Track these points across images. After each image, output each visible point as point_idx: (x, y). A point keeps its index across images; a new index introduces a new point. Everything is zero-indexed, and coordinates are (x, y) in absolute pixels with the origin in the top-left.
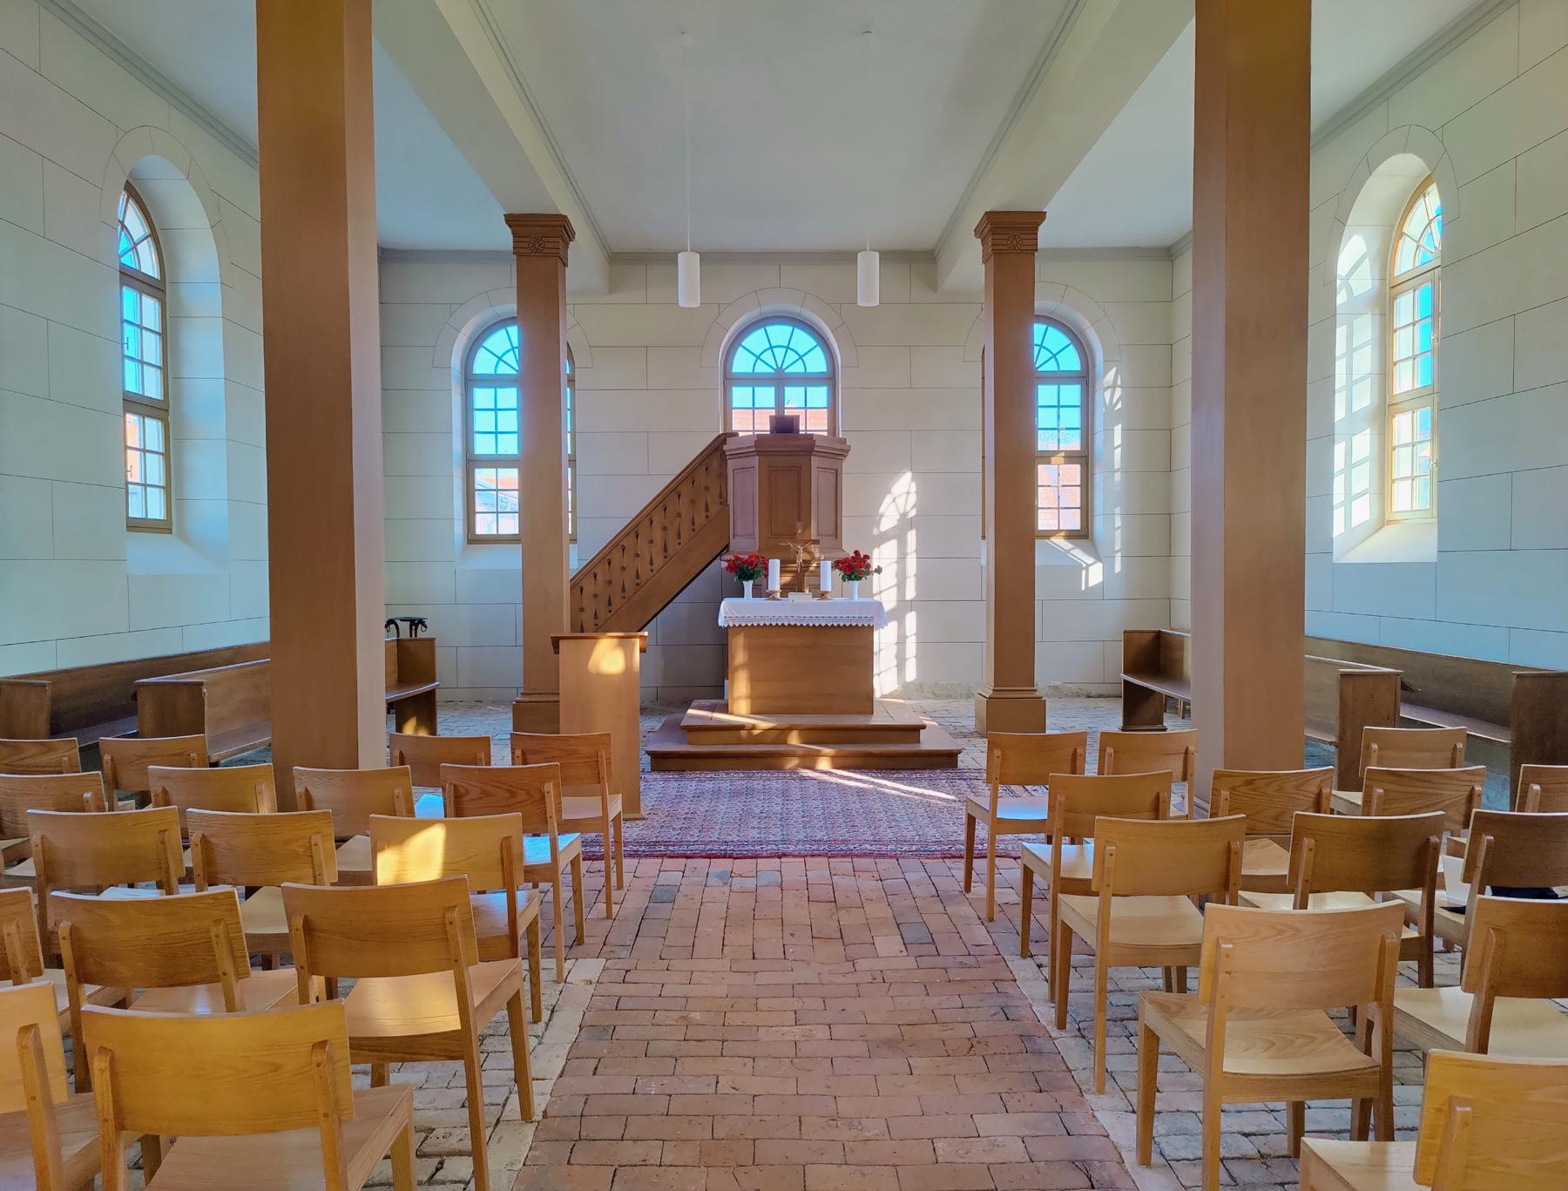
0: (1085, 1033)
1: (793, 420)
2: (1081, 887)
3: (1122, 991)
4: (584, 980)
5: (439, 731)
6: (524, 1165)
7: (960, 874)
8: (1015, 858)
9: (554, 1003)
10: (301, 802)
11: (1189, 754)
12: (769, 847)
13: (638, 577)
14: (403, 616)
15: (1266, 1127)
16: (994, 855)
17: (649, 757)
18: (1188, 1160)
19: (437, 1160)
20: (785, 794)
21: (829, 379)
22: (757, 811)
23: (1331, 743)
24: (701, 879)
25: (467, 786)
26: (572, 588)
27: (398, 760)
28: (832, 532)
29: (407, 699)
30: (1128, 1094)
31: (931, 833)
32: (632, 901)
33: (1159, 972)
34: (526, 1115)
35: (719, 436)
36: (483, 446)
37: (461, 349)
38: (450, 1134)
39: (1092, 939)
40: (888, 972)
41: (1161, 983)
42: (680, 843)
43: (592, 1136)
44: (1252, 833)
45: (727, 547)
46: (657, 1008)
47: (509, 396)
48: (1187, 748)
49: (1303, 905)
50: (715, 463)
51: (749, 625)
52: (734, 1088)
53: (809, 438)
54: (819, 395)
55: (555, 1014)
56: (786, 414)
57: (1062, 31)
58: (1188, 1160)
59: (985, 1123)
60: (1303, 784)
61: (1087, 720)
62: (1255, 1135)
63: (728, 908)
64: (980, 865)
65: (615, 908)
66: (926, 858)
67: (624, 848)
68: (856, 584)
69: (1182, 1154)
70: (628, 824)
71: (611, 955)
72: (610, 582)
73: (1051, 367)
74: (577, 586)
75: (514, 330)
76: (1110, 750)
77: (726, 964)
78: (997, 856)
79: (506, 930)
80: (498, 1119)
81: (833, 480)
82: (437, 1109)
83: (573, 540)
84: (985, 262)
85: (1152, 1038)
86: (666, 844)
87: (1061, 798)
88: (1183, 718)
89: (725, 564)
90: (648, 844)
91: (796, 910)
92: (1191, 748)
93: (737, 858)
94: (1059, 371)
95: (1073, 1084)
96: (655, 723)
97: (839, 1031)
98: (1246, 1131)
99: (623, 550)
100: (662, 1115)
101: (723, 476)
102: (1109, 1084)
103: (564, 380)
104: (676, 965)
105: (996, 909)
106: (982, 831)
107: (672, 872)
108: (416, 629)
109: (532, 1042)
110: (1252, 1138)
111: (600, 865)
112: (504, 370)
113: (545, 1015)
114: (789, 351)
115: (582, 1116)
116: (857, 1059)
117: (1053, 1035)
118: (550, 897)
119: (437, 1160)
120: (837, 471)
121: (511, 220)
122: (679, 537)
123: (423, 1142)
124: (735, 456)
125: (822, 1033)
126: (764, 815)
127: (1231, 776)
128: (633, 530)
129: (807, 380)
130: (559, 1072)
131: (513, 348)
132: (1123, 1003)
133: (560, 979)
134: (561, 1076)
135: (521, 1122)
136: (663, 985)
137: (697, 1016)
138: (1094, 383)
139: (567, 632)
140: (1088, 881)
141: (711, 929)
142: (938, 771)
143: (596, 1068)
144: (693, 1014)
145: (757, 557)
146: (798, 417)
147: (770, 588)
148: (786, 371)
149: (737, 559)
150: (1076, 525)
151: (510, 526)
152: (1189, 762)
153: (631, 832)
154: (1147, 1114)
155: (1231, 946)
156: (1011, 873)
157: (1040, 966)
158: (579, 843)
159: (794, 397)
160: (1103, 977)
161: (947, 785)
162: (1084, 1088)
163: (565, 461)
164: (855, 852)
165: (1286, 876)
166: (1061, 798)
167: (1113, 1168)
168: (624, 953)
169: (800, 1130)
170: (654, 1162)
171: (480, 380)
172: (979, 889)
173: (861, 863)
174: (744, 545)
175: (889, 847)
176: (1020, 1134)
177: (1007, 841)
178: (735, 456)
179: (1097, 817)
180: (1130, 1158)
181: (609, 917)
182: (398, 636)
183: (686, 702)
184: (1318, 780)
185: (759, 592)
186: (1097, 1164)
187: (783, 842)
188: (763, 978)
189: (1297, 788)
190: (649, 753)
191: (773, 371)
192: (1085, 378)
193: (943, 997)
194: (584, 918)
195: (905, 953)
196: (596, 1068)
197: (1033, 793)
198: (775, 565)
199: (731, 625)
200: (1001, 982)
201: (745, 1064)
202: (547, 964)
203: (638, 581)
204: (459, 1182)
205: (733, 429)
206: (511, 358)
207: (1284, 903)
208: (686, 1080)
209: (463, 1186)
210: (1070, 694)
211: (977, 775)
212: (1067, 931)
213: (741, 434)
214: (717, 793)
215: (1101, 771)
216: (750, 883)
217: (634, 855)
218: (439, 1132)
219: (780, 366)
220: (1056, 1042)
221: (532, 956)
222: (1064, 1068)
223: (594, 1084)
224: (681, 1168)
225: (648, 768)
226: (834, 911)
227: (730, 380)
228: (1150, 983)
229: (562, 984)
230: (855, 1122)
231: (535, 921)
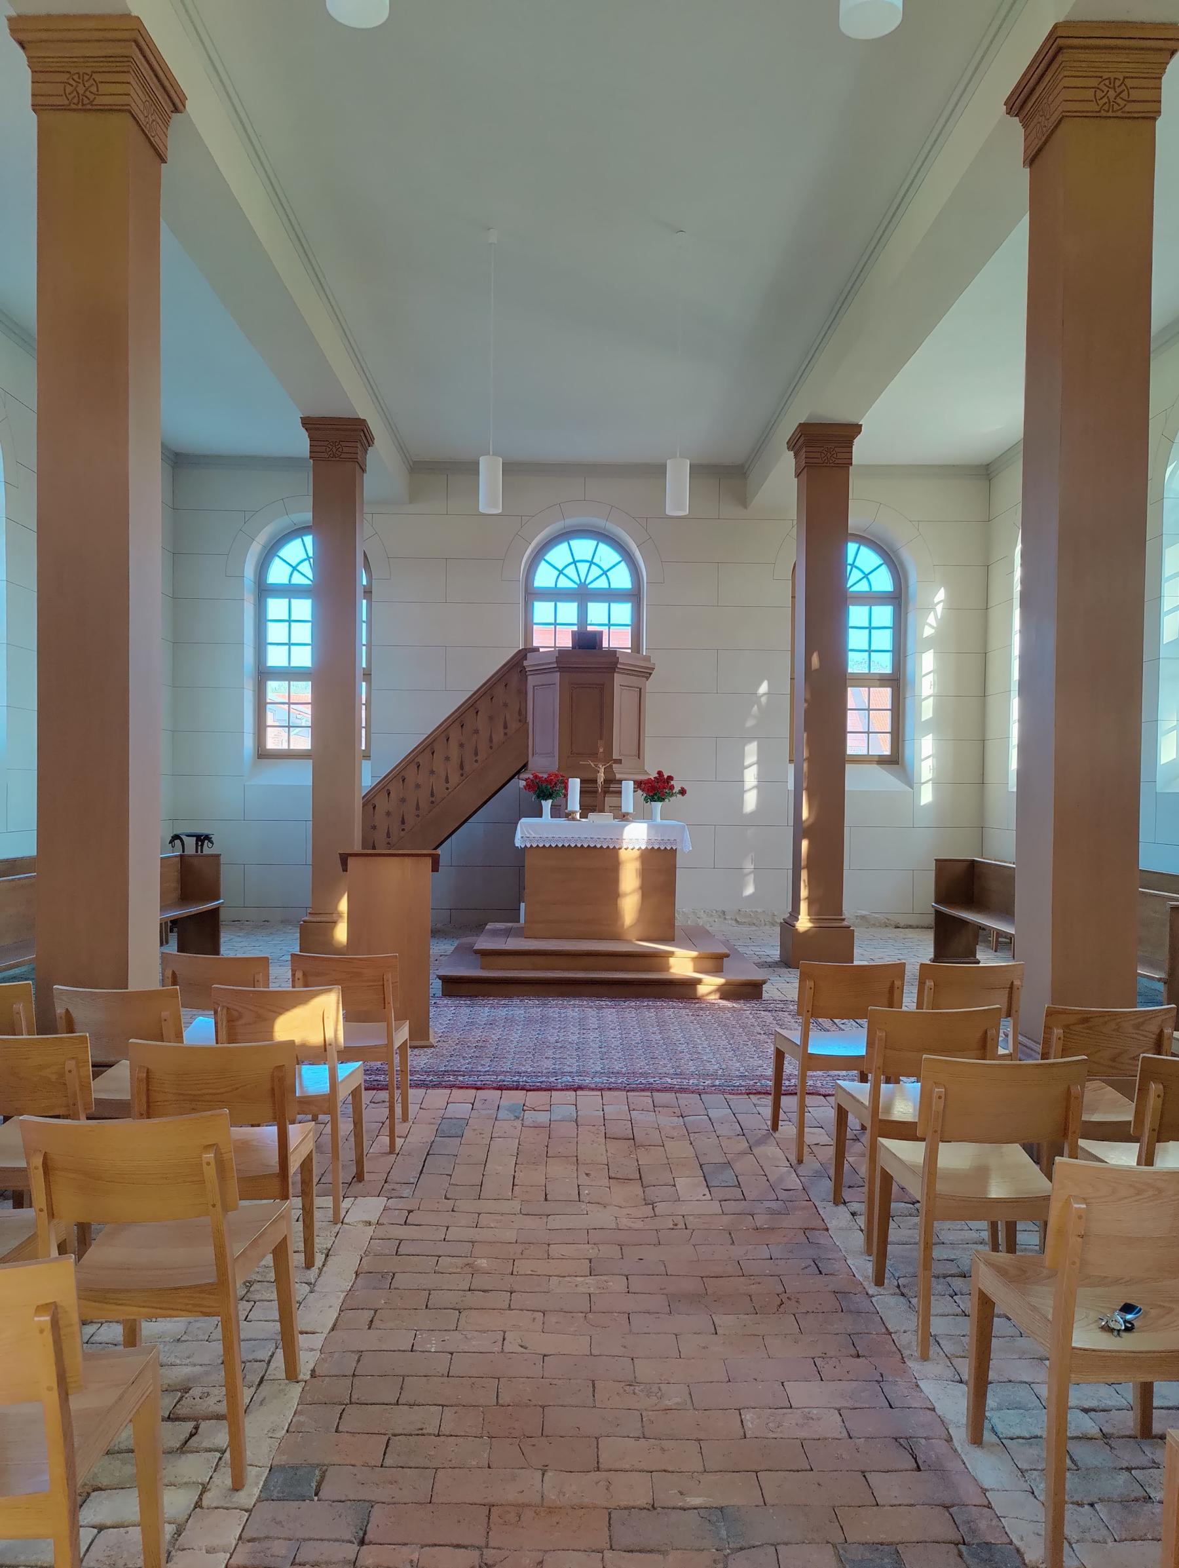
0: (905, 1291)
1: (596, 635)
2: (904, 1131)
3: (943, 1243)
4: (363, 1222)
5: (222, 952)
6: (287, 1431)
7: (767, 1112)
8: (825, 1096)
9: (329, 1246)
10: (61, 1024)
11: (1015, 988)
12: (564, 1079)
13: (432, 795)
14: (189, 831)
15: (1108, 1402)
16: (802, 1093)
17: (441, 981)
18: (1023, 1438)
19: (191, 1424)
20: (582, 1024)
21: (634, 596)
22: (552, 1040)
23: (1160, 980)
24: (492, 1111)
25: (240, 1009)
26: (364, 805)
27: (170, 980)
28: (635, 752)
29: (189, 917)
30: (955, 1361)
31: (736, 1067)
32: (417, 1135)
33: (984, 1225)
34: (291, 1373)
35: (520, 651)
36: (276, 658)
37: (254, 563)
38: (208, 1394)
39: (916, 1190)
40: (690, 1218)
41: (985, 1235)
42: (470, 1073)
43: (363, 1400)
44: (1092, 1074)
45: (525, 766)
46: (441, 1254)
47: (303, 608)
48: (1012, 982)
49: (1147, 1158)
50: (515, 679)
51: (547, 845)
52: (522, 1346)
53: (612, 653)
54: (623, 612)
55: (330, 1258)
56: (588, 629)
57: (868, 260)
58: (1023, 1438)
59: (799, 1392)
60: (1143, 1023)
61: (897, 951)
62: (1094, 1410)
63: (519, 1144)
64: (789, 1103)
65: (399, 1142)
66: (730, 1094)
67: (410, 1078)
68: (659, 804)
69: (1017, 1432)
70: (416, 1051)
71: (394, 1194)
72: (403, 800)
73: (863, 587)
74: (369, 802)
75: (309, 539)
76: (930, 983)
77: (515, 1205)
78: (807, 1093)
79: (277, 1169)
80: (262, 1378)
81: (637, 700)
82: (195, 1365)
83: (367, 756)
84: (798, 475)
85: (986, 1304)
86: (455, 1073)
87: (880, 1034)
88: (996, 951)
89: (523, 783)
90: (436, 1073)
91: (594, 1149)
92: (1017, 983)
93: (530, 1090)
94: (870, 592)
95: (894, 1349)
96: (441, 948)
97: (637, 1284)
98: (1086, 1406)
99: (418, 767)
100: (443, 1376)
101: (522, 692)
102: (934, 1349)
103: (360, 592)
104: (462, 1205)
105: (806, 1149)
106: (791, 1067)
107: (460, 1103)
108: (202, 845)
109: (300, 1291)
110: (1092, 1414)
111: (384, 1095)
112: (298, 579)
113: (319, 1259)
114: (593, 566)
115: (354, 1375)
116: (657, 1315)
117: (870, 1292)
118: (328, 1129)
119: (191, 1424)
120: (640, 689)
121: (308, 423)
122: (476, 754)
123: (177, 1403)
124: (538, 672)
125: (618, 1284)
126: (559, 1045)
127: (1065, 1013)
128: (428, 747)
129: (610, 596)
130: (330, 1325)
131: (308, 558)
132: (945, 1257)
133: (337, 1219)
134: (333, 1329)
135: (287, 1382)
136: (448, 1227)
137: (483, 1263)
138: (907, 603)
139: (357, 848)
140: (913, 1125)
141: (501, 1166)
142: (742, 1001)
143: (372, 1321)
144: (479, 1261)
145: (556, 776)
146: (601, 633)
147: (569, 808)
148: (589, 586)
149: (536, 777)
150: (887, 751)
151: (303, 741)
152: (1015, 998)
153: (420, 1060)
154: (980, 1386)
155: (1084, 1206)
156: (822, 1112)
157: (853, 1214)
158: (361, 1071)
159: (597, 613)
160: (928, 1231)
161: (751, 1017)
162: (906, 1353)
163: (359, 674)
164: (654, 1086)
165: (1130, 1122)
166: (880, 1034)
167: (940, 1445)
168: (406, 1192)
169: (594, 1396)
170: (431, 1432)
171: (272, 590)
172: (788, 1129)
173: (661, 1097)
174: (542, 764)
175: (691, 1081)
176: (837, 1406)
177: (816, 1078)
178: (538, 672)
179: (924, 1056)
180: (960, 1435)
181: (392, 1150)
182: (183, 852)
183: (480, 926)
184: (1159, 1019)
185: (557, 812)
186: (923, 1441)
187: (580, 1073)
188: (555, 1222)
189: (1137, 1027)
190: (440, 977)
191: (576, 586)
192: (898, 599)
193: (750, 1247)
194: (365, 1154)
195: (708, 1197)
196: (372, 1321)
197: (842, 1026)
198: (575, 785)
199: (528, 846)
200: (813, 1230)
201: (534, 1319)
202: (323, 1203)
203: (433, 799)
204: (216, 1450)
205: (534, 645)
206: (306, 568)
207: (1123, 1156)
208: (469, 1336)
209: (218, 1455)
210: (878, 925)
211: (782, 1006)
212: (887, 1179)
213: (541, 650)
214: (510, 1021)
215: (919, 1006)
216: (543, 1118)
217: (423, 1085)
218: (196, 1391)
219: (579, 582)
220: (874, 1299)
221: (306, 1193)
222: (884, 1330)
223: (369, 1340)
224: (462, 1439)
225: (439, 993)
226: (632, 1149)
227: (532, 595)
228: (974, 1235)
229: (339, 1225)
230: (655, 1389)
231: (309, 1158)
